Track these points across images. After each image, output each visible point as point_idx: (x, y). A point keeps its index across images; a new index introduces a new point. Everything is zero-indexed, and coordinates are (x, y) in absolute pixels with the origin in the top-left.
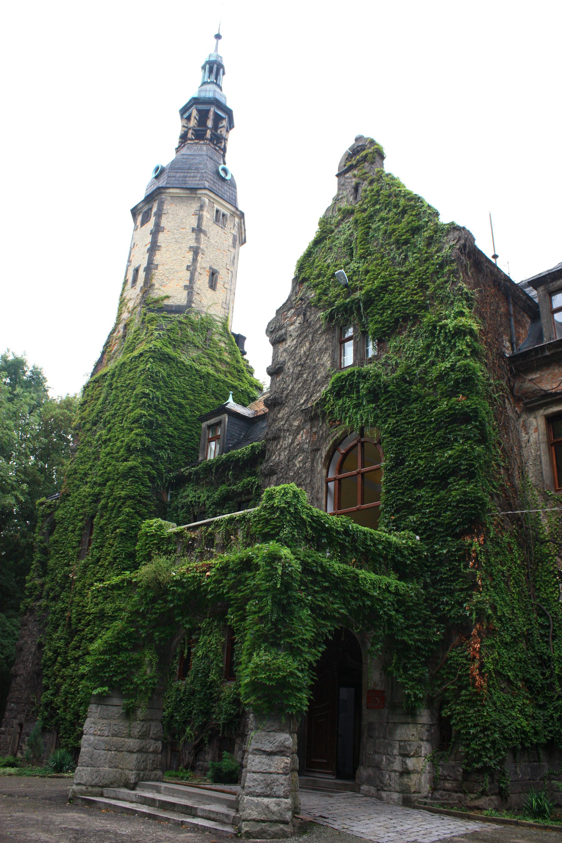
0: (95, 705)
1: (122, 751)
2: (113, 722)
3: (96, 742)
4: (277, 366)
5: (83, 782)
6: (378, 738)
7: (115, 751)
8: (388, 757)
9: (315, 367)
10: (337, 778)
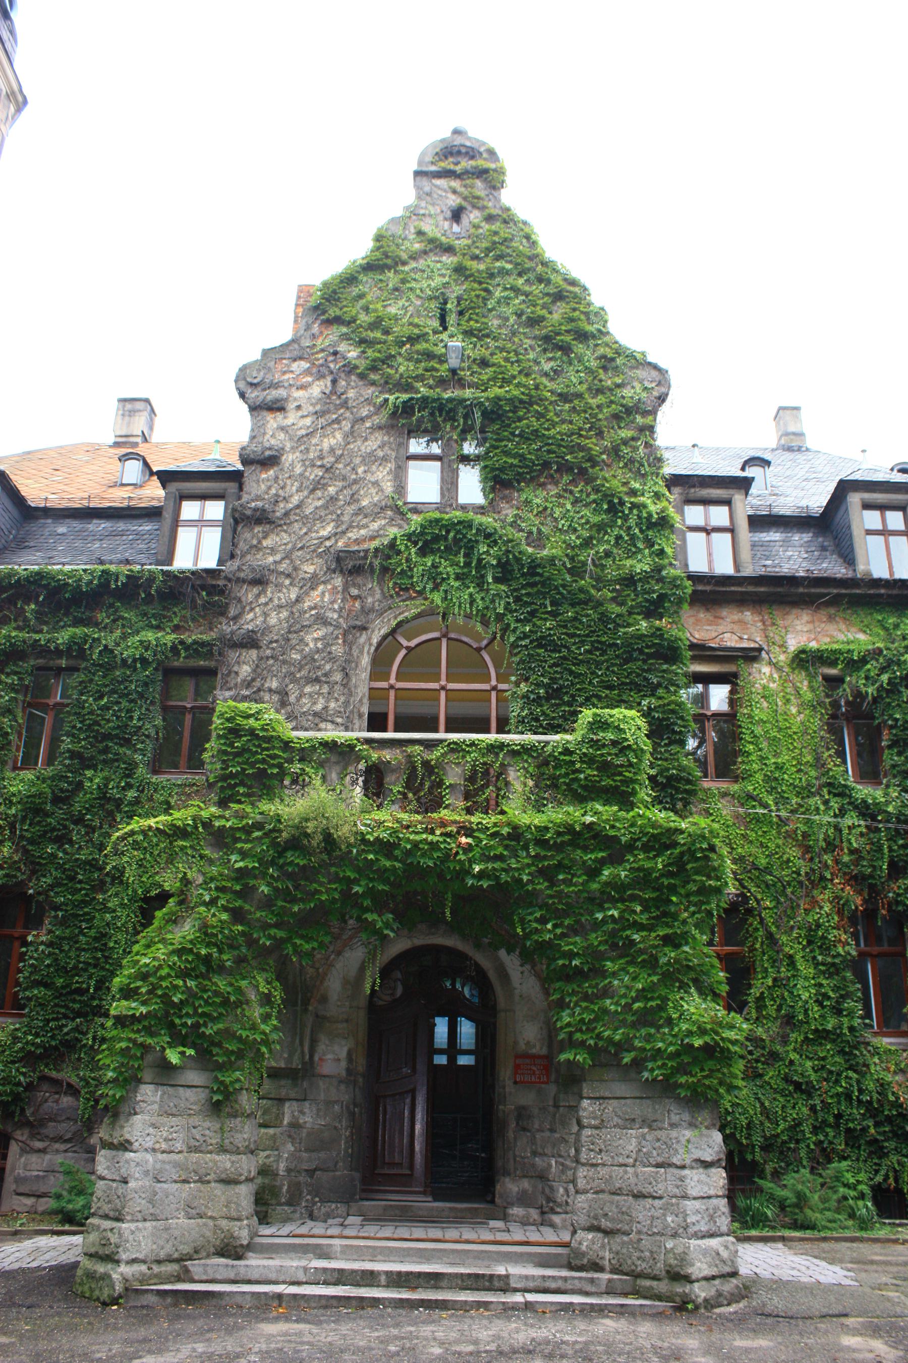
0: (152, 1087)
1: (209, 1182)
2: (195, 1120)
3: (158, 1166)
4: (268, 453)
5: (141, 1256)
6: (541, 1130)
7: (195, 1182)
8: (560, 1160)
9: (355, 482)
10: (435, 1200)
